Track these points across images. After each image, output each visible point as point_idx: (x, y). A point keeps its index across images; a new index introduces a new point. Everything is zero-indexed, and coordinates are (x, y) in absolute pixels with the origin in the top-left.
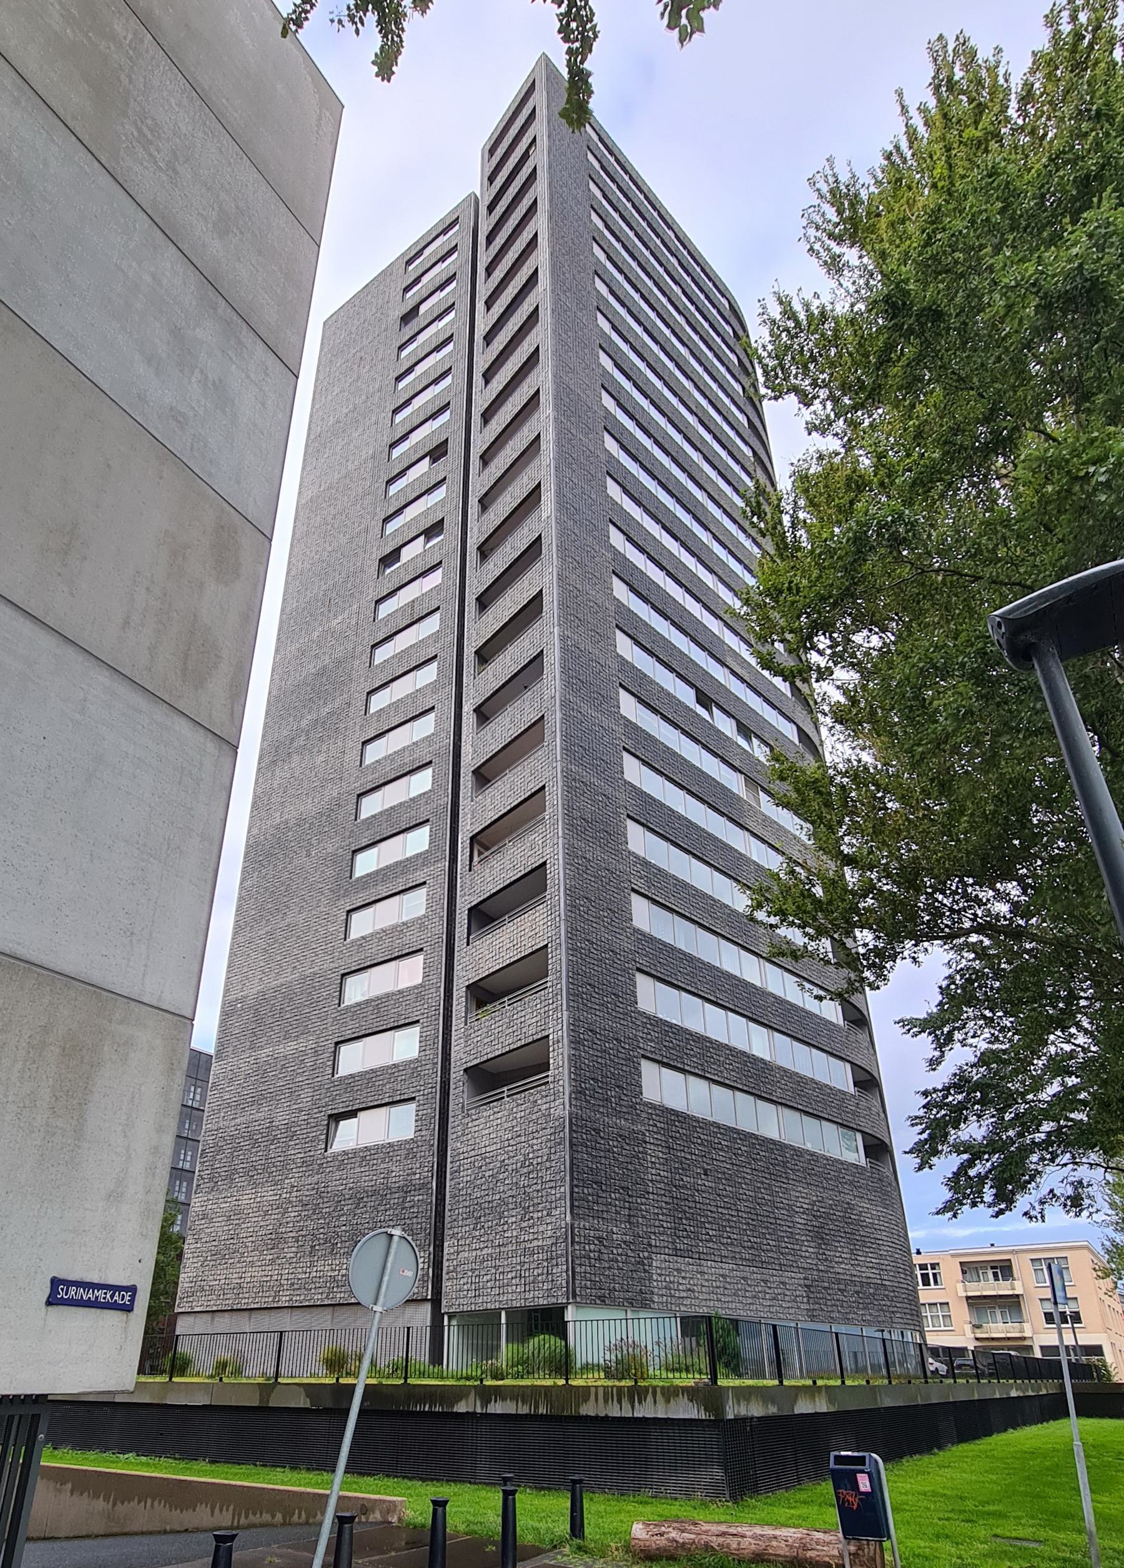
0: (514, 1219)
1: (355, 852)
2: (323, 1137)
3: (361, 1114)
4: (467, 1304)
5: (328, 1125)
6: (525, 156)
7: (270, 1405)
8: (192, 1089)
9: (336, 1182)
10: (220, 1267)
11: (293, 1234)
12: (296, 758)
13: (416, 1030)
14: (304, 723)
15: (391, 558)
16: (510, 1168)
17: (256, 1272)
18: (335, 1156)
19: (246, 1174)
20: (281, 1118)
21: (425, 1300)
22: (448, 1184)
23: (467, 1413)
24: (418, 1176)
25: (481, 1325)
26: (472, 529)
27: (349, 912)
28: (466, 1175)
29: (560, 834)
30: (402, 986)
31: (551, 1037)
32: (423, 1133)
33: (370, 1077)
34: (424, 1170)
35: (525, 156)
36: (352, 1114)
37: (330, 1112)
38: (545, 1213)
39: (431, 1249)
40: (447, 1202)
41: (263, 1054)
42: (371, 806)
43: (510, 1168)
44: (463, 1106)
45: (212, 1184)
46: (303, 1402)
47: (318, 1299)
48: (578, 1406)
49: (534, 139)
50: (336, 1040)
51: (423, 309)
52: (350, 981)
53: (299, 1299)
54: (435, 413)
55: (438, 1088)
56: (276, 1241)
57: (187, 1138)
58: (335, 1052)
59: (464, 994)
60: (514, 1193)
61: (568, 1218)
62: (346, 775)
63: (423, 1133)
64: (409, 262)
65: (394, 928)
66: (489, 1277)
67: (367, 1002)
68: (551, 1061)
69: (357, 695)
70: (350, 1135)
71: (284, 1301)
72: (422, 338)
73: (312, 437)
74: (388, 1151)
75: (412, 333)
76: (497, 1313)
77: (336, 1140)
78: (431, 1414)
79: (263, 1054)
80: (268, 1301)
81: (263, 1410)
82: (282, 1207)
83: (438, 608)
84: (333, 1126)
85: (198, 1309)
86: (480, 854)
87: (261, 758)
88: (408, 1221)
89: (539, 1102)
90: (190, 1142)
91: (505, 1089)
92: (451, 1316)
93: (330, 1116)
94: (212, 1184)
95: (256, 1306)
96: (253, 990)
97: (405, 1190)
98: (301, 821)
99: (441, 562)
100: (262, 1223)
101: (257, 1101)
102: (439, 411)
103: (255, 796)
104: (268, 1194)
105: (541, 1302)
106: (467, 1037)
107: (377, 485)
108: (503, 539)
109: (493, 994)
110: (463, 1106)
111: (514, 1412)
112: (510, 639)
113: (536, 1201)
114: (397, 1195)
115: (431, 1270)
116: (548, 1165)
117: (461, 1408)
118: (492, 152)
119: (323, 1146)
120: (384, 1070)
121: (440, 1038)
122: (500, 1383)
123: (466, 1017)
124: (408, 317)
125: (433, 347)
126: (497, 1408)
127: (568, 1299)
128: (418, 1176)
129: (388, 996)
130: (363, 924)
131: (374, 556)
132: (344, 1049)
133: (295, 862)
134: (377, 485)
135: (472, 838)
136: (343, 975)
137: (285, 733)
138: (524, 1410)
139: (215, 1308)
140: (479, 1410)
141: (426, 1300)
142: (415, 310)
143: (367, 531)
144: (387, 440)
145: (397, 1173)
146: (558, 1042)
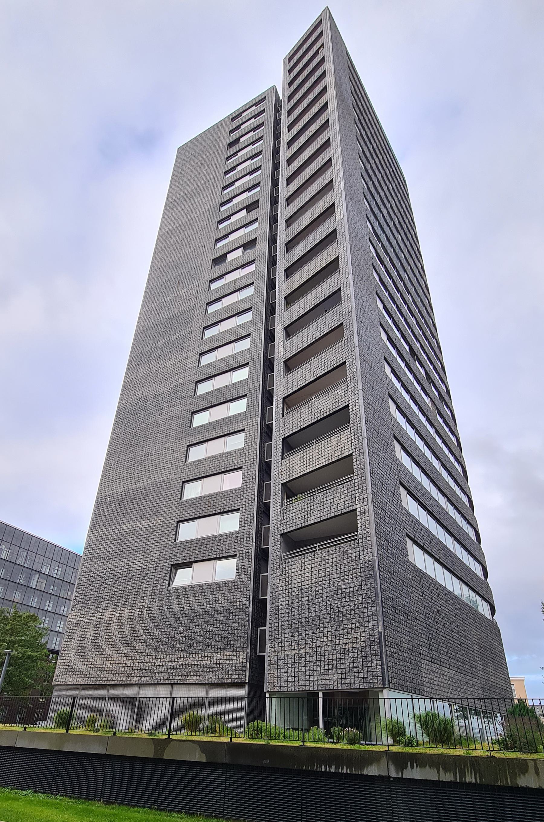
0: (329, 629)
1: (193, 413)
2: (168, 578)
3: (195, 565)
4: (288, 685)
5: (171, 570)
6: (317, 53)
7: (165, 757)
8: (57, 568)
9: (176, 605)
10: (87, 657)
11: (144, 638)
12: (153, 362)
13: (237, 515)
14: (160, 344)
15: (220, 260)
16: (324, 595)
17: (114, 661)
18: (176, 589)
19: (110, 599)
20: (136, 565)
21: (244, 683)
22: (268, 607)
23: (380, 777)
24: (238, 603)
25: (303, 703)
26: (280, 236)
27: (188, 446)
28: (284, 601)
29: (360, 388)
30: (225, 489)
31: (358, 510)
32: (243, 577)
33: (202, 542)
34: (245, 599)
35: (317, 53)
36: (188, 565)
37: (172, 563)
38: (358, 625)
39: (249, 650)
40: (268, 618)
41: (125, 528)
42: (204, 388)
43: (324, 595)
44: (281, 557)
45: (84, 605)
46: (199, 757)
47: (161, 679)
48: (514, 777)
49: (323, 44)
50: (178, 520)
51: (242, 140)
52: (187, 486)
53: (145, 679)
54: (250, 188)
55: (254, 549)
56: (131, 641)
57: (51, 594)
58: (177, 527)
59: (280, 489)
60: (328, 611)
61: (381, 628)
62: (188, 371)
63: (243, 577)
64: (233, 119)
65: (221, 455)
66: (307, 668)
67: (201, 498)
68: (359, 525)
69: (196, 329)
70: (184, 578)
71: (135, 680)
72: (240, 154)
73: (169, 202)
74: (215, 587)
75: (235, 151)
76: (314, 695)
77: (175, 580)
78: (337, 775)
79: (125, 528)
80: (122, 679)
81: (158, 762)
82: (136, 621)
83: (253, 283)
84: (173, 571)
85: (70, 683)
86: (287, 410)
87: (129, 363)
88: (230, 632)
89: (349, 552)
90: (53, 596)
91: (317, 545)
92: (272, 694)
93: (172, 565)
94: (84, 605)
95: (113, 683)
96: (119, 489)
97: (228, 612)
98: (156, 396)
99: (255, 260)
100: (120, 630)
101: (119, 555)
102: (253, 187)
103: (125, 383)
104: (126, 612)
105: (357, 686)
106: (283, 515)
107: (211, 223)
108: (297, 243)
109: (293, 493)
110: (281, 557)
111: (437, 779)
112: (313, 287)
113: (349, 617)
114: (222, 615)
115: (248, 664)
116: (360, 592)
117: (372, 771)
118: (290, 59)
119: (167, 583)
120: (213, 538)
121: (255, 519)
122: (356, 747)
123: (282, 502)
124: (230, 145)
125: (249, 156)
126: (414, 773)
127: (384, 684)
128: (238, 603)
129: (216, 494)
130: (197, 454)
131: (209, 258)
132: (182, 526)
133: (152, 418)
134: (211, 223)
135: (284, 399)
136: (184, 482)
137: (147, 349)
138: (447, 777)
139: (82, 683)
140: (393, 774)
141: (244, 683)
142: (237, 141)
143: (204, 246)
144: (219, 201)
145: (223, 601)
146: (365, 513)
